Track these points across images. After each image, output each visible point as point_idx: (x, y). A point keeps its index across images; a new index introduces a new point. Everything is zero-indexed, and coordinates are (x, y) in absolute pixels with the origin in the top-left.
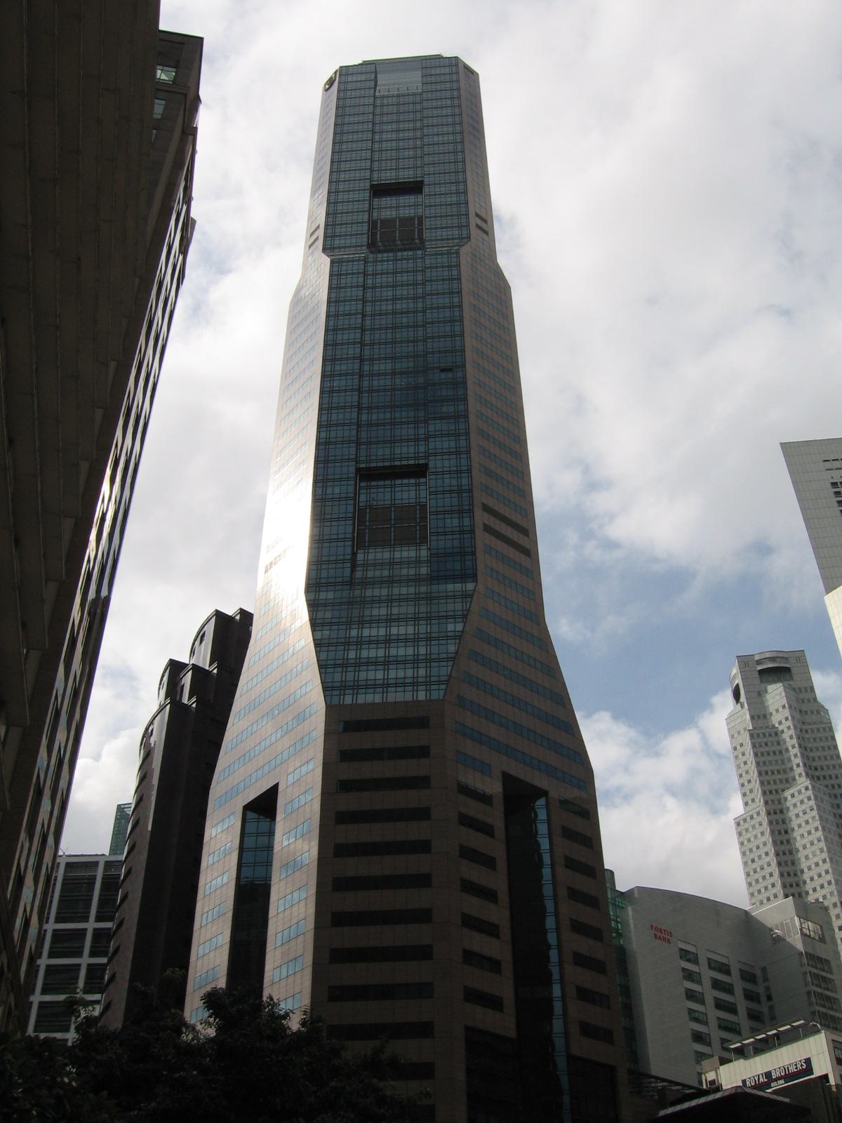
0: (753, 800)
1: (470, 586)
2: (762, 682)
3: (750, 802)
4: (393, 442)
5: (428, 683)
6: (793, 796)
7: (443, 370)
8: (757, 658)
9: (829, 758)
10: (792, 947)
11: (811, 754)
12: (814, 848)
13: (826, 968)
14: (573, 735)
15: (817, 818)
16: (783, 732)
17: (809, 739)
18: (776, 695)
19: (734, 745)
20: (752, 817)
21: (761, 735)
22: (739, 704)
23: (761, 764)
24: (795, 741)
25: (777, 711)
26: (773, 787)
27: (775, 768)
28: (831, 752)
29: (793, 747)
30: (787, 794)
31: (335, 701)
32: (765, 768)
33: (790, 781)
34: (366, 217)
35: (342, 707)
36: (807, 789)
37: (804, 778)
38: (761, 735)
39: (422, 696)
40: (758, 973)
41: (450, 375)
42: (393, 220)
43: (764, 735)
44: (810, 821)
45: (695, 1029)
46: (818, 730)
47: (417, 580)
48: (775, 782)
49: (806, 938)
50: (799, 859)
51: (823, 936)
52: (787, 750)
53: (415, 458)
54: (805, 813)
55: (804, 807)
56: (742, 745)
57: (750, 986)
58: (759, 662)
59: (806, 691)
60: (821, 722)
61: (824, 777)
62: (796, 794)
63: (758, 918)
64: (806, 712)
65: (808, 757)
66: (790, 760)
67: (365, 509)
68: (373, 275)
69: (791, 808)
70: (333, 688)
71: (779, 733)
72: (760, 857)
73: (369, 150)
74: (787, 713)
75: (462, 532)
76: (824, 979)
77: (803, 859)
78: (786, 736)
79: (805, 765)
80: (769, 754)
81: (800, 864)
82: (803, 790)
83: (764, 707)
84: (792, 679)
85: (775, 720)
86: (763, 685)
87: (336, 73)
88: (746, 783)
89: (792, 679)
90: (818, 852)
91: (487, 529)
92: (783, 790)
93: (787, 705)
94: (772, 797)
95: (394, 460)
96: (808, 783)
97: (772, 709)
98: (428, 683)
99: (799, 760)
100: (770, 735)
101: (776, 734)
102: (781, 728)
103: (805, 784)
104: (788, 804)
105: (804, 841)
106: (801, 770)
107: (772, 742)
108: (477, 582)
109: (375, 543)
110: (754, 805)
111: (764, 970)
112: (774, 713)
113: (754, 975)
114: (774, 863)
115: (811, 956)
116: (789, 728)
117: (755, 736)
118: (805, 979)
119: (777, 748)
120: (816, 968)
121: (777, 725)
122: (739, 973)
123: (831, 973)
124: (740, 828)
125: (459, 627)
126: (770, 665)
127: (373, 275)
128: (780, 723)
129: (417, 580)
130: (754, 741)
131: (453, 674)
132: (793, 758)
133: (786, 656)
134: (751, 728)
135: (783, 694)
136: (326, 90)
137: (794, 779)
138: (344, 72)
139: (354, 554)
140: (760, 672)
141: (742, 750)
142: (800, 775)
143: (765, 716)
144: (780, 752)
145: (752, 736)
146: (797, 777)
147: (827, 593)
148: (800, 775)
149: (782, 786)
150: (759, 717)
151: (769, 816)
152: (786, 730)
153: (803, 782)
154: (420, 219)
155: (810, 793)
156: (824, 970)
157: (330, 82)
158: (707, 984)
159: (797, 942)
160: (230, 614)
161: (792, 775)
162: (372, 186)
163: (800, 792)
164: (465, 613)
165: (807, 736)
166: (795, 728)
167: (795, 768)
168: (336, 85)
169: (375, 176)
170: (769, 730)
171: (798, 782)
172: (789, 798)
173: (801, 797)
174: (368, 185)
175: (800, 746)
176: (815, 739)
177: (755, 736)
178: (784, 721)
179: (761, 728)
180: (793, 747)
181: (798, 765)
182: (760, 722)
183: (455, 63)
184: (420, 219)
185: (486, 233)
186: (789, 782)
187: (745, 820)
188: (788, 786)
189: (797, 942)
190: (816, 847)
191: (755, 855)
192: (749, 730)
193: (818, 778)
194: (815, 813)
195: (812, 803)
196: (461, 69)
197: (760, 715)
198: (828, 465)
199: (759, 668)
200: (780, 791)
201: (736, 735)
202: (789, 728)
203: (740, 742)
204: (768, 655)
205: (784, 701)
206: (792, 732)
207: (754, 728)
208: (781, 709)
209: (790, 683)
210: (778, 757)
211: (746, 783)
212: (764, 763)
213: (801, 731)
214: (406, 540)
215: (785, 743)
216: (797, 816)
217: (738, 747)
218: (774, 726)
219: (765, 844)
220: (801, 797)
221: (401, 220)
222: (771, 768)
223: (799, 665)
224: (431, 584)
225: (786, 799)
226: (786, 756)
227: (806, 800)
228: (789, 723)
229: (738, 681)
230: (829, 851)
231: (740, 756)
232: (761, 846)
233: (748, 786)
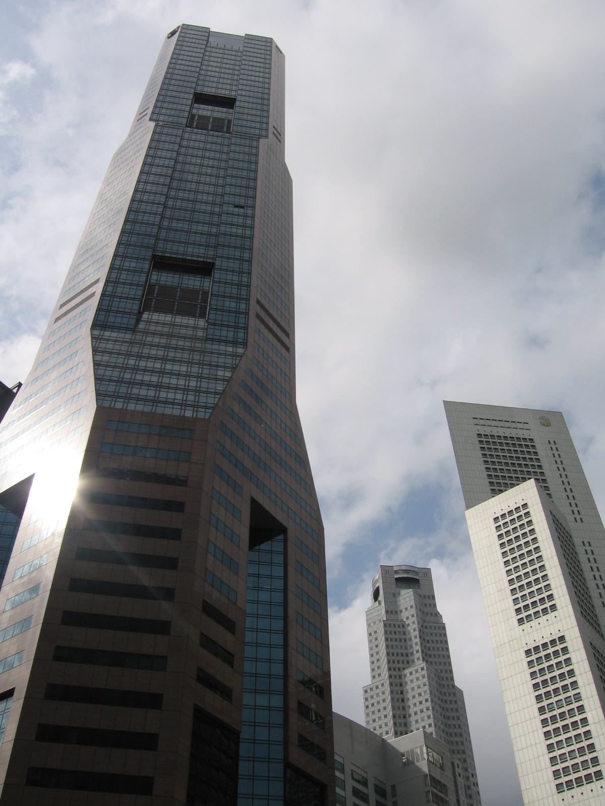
0: (379, 675)
1: (240, 350)
2: (397, 587)
3: (377, 676)
4: (187, 243)
5: (195, 406)
6: (411, 673)
7: (236, 206)
8: (395, 569)
9: (440, 649)
10: (419, 770)
11: (428, 645)
12: (423, 715)
13: (444, 791)
14: (311, 495)
15: (428, 692)
16: (409, 625)
17: (427, 633)
18: (407, 597)
19: (370, 632)
20: (377, 687)
21: (392, 626)
22: (377, 602)
23: (390, 647)
24: (417, 633)
25: (406, 609)
26: (396, 665)
27: (400, 651)
28: (442, 645)
29: (415, 637)
30: (407, 672)
31: (106, 404)
32: (393, 651)
33: (410, 662)
34: (143, 279)
35: (110, 409)
36: (422, 669)
37: (421, 662)
38: (392, 626)
39: (189, 414)
40: (389, 790)
41: (241, 210)
42: (209, 117)
43: (394, 626)
44: (423, 694)
45: (356, 803)
46: (435, 628)
47: (194, 338)
48: (398, 662)
49: (431, 764)
50: (411, 722)
51: (443, 765)
52: (410, 639)
53: (204, 257)
54: (419, 687)
55: (419, 683)
56: (376, 632)
57: (381, 799)
58: (396, 572)
59: (429, 598)
60: (437, 623)
61: (436, 663)
62: (414, 672)
63: (393, 744)
64: (427, 614)
65: (425, 646)
66: (411, 647)
67: (155, 286)
68: (164, 240)
69: (409, 683)
70: (105, 395)
71: (406, 626)
72: (380, 718)
73: (156, 225)
74: (413, 611)
75: (238, 312)
76: (442, 799)
77: (414, 723)
78: (410, 629)
79: (422, 651)
80: (396, 640)
81: (410, 726)
82: (420, 670)
83: (397, 606)
84: (419, 588)
85: (404, 616)
86: (398, 589)
87: (178, 28)
88: (375, 661)
89: (419, 588)
90: (426, 718)
91: (258, 316)
92: (404, 669)
93: (414, 606)
94: (395, 673)
95: (186, 255)
96: (424, 665)
97: (402, 607)
98: (195, 406)
99: (418, 647)
100: (399, 627)
101: (403, 626)
102: (407, 622)
103: (422, 666)
104: (407, 679)
105: (415, 709)
106: (419, 655)
107: (400, 632)
108: (246, 348)
109: (158, 310)
110: (380, 678)
111: (393, 787)
112: (404, 610)
113: (385, 791)
114: (391, 723)
115: (433, 779)
116: (414, 623)
117: (388, 625)
118: (427, 797)
119: (403, 637)
120: (436, 789)
121: (405, 620)
122: (374, 788)
123: (446, 794)
124: (367, 695)
125: (228, 374)
126: (405, 575)
127: (164, 240)
128: (407, 618)
129: (194, 338)
130: (386, 629)
131: (219, 404)
132: (414, 645)
133: (416, 570)
134: (385, 619)
135: (413, 597)
136: (169, 38)
137: (413, 661)
138: (185, 28)
139: (140, 314)
140: (397, 579)
141: (375, 636)
142: (418, 659)
143: (396, 612)
144: (405, 640)
145: (385, 625)
146: (416, 660)
147: (467, 509)
148: (418, 659)
149: (402, 666)
150: (392, 612)
151: (392, 687)
152: (411, 624)
153: (420, 664)
154: (229, 122)
155: (425, 672)
156: (442, 792)
157: (173, 34)
158: (349, 790)
159: (424, 766)
160: (9, 387)
161: (411, 658)
162: (154, 257)
163: (417, 671)
164: (234, 366)
165: (426, 631)
166: (418, 623)
167: (415, 653)
168: (177, 34)
169: (161, 245)
170: (399, 623)
171: (416, 664)
172: (408, 675)
173: (418, 675)
174: (192, 91)
175: (420, 637)
176: (432, 634)
177: (388, 625)
178: (410, 617)
179: (392, 620)
180: (415, 637)
181: (417, 651)
182: (392, 615)
183: (268, 43)
184: (229, 122)
185: (280, 141)
186: (409, 663)
187: (371, 689)
188: (408, 666)
189: (424, 766)
190: (425, 714)
191: (375, 717)
192: (383, 621)
193: (431, 663)
194: (427, 688)
195: (426, 680)
196: (274, 48)
197: (392, 611)
198: (477, 421)
199: (397, 576)
200: (401, 669)
201: (372, 625)
202: (414, 623)
203: (375, 630)
204: (404, 568)
205: (412, 603)
206: (416, 626)
207: (387, 620)
208: (409, 608)
209: (418, 590)
210: (403, 644)
211: (375, 661)
212: (392, 647)
213: (422, 626)
214: (189, 312)
215: (409, 633)
216: (413, 689)
217: (373, 634)
218: (402, 620)
219: (385, 708)
220: (418, 675)
221: (215, 119)
222: (397, 651)
223: (426, 578)
224: (205, 343)
225: (405, 676)
226: (409, 643)
227: (421, 678)
228: (415, 619)
229: (380, 584)
230: (434, 718)
231: (374, 640)
232: (382, 710)
233: (376, 664)
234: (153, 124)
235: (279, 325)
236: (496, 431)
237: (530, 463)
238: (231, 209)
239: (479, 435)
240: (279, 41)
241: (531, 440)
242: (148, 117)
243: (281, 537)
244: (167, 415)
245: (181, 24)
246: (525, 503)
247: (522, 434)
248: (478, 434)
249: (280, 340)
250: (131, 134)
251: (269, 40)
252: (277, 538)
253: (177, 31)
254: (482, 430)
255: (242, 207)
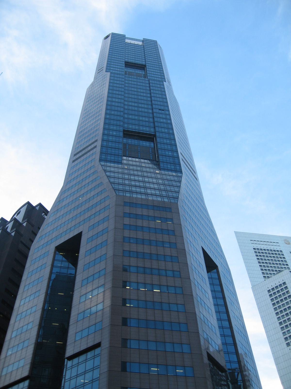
53: (149, 132)
136: (105, 39)
157: (107, 37)
162: (124, 131)
168: (110, 38)
196: (159, 47)
198: (252, 242)
234: (109, 74)
235: (191, 167)
236: (262, 247)
237: (282, 263)
238: (158, 111)
239: (254, 249)
240: (160, 43)
241: (281, 251)
242: (104, 70)
243: (215, 271)
244: (155, 200)
245: (111, 33)
246: (284, 282)
247: (276, 248)
248: (254, 248)
249: (193, 174)
250: (96, 78)
251: (155, 41)
252: (212, 271)
253: (109, 36)
254: (256, 246)
255: (163, 110)
